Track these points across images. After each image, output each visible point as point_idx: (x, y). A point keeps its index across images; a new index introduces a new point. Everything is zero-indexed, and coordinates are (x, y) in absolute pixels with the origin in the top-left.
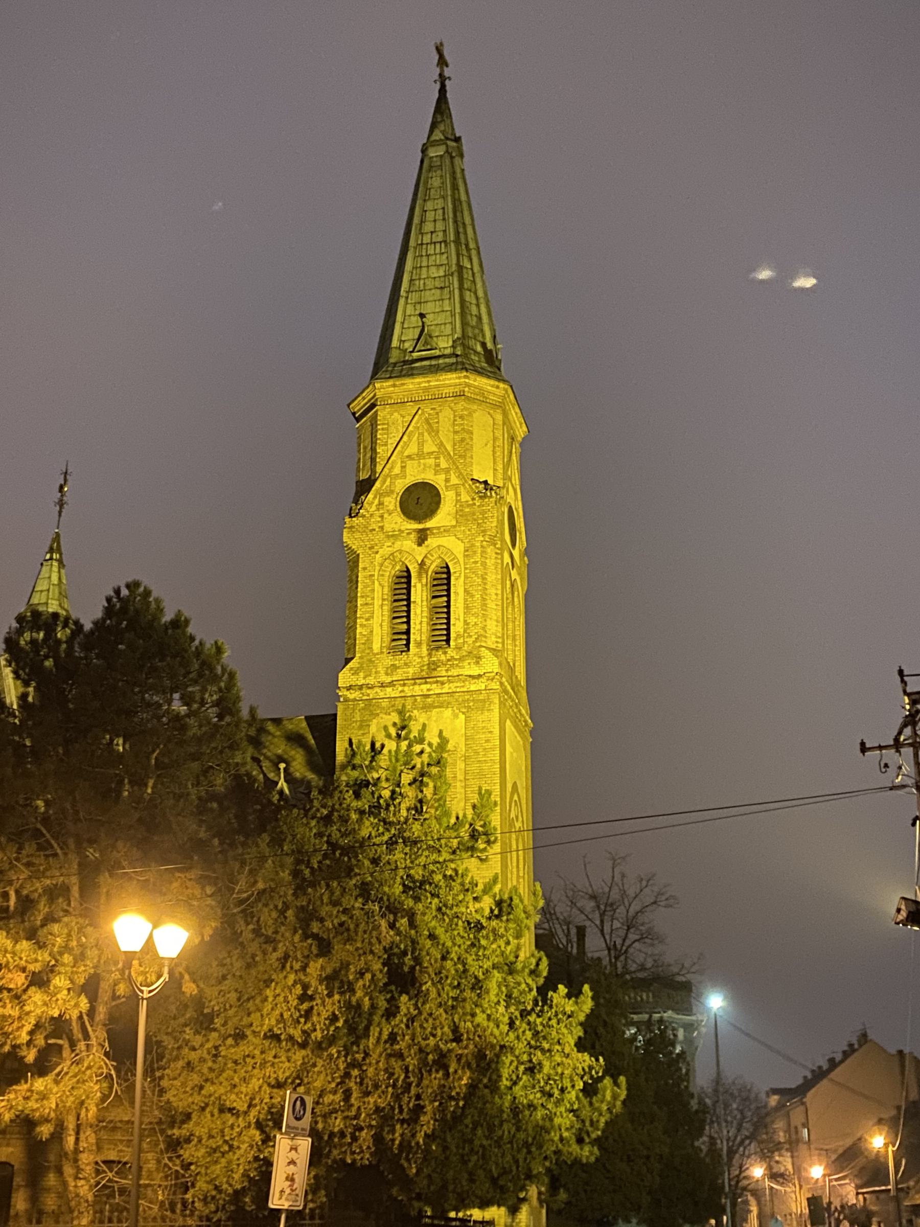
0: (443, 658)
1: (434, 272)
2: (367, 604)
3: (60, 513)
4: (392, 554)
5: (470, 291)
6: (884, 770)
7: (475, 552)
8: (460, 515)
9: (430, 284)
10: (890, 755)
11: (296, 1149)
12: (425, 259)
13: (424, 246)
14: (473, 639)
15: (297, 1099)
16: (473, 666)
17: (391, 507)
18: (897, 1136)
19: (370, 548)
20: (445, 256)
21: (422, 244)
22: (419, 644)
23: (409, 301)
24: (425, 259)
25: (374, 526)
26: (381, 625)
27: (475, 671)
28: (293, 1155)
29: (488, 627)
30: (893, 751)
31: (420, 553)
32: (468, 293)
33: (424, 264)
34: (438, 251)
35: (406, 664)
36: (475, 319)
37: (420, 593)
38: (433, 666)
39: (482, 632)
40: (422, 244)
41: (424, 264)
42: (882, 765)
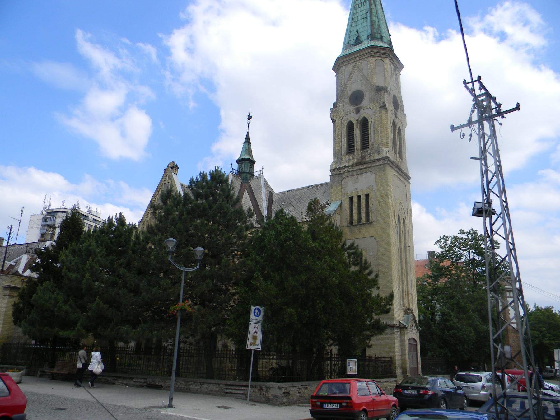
0: (366, 154)
1: (361, 13)
2: (339, 138)
3: (249, 126)
4: (347, 118)
5: (375, 16)
6: (462, 137)
7: (377, 112)
8: (372, 100)
9: (360, 18)
10: (467, 131)
11: (257, 327)
12: (358, 9)
13: (358, 5)
14: (377, 145)
15: (256, 309)
16: (377, 155)
17: (346, 102)
18: (168, 241)
19: (339, 118)
20: (365, 7)
21: (357, 5)
22: (358, 150)
23: (352, 26)
24: (358, 9)
25: (341, 110)
26: (344, 145)
27: (379, 157)
28: (256, 330)
29: (383, 140)
30: (468, 127)
31: (357, 117)
32: (374, 17)
33: (358, 11)
34: (362, 5)
35: (353, 158)
36: (377, 26)
37: (357, 133)
38: (363, 157)
39: (381, 142)
40: (357, 5)
41: (358, 11)
42: (462, 134)
